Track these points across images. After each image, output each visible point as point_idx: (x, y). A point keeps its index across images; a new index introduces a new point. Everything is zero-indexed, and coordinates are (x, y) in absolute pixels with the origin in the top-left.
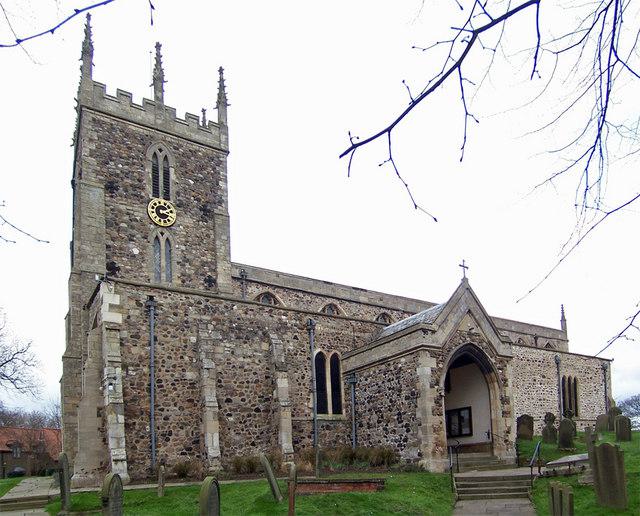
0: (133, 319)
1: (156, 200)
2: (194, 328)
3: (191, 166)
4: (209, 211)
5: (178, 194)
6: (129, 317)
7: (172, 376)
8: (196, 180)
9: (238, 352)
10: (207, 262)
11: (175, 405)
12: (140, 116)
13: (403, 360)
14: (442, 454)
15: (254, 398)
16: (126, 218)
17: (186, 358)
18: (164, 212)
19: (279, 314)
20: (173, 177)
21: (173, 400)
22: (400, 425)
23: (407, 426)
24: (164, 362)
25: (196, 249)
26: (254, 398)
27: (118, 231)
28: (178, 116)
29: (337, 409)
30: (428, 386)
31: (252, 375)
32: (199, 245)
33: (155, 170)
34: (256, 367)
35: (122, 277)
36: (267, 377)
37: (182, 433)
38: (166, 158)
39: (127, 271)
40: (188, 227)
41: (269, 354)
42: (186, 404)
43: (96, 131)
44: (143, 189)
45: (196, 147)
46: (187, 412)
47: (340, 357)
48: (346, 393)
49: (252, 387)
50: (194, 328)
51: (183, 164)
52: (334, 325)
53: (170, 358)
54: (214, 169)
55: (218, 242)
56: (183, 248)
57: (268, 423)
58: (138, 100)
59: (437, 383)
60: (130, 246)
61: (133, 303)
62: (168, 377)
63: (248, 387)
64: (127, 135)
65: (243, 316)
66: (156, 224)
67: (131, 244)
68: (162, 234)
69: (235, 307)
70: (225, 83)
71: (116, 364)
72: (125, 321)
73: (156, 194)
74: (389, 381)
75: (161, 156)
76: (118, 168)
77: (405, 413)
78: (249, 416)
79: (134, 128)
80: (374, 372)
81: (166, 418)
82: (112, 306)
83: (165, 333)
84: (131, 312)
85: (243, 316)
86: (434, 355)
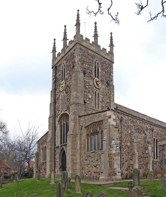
5: (101, 77)
6: (117, 123)
8: (105, 72)
20: (100, 70)
35: (87, 106)
36: (144, 146)
37: (126, 163)
39: (88, 104)
41: (145, 138)
45: (105, 60)
47: (158, 140)
50: (130, 128)
51: (102, 66)
54: (110, 68)
56: (102, 96)
60: (89, 95)
61: (118, 118)
66: (96, 87)
71: (118, 139)
72: (116, 125)
79: (90, 52)
81: (123, 159)
82: (114, 119)
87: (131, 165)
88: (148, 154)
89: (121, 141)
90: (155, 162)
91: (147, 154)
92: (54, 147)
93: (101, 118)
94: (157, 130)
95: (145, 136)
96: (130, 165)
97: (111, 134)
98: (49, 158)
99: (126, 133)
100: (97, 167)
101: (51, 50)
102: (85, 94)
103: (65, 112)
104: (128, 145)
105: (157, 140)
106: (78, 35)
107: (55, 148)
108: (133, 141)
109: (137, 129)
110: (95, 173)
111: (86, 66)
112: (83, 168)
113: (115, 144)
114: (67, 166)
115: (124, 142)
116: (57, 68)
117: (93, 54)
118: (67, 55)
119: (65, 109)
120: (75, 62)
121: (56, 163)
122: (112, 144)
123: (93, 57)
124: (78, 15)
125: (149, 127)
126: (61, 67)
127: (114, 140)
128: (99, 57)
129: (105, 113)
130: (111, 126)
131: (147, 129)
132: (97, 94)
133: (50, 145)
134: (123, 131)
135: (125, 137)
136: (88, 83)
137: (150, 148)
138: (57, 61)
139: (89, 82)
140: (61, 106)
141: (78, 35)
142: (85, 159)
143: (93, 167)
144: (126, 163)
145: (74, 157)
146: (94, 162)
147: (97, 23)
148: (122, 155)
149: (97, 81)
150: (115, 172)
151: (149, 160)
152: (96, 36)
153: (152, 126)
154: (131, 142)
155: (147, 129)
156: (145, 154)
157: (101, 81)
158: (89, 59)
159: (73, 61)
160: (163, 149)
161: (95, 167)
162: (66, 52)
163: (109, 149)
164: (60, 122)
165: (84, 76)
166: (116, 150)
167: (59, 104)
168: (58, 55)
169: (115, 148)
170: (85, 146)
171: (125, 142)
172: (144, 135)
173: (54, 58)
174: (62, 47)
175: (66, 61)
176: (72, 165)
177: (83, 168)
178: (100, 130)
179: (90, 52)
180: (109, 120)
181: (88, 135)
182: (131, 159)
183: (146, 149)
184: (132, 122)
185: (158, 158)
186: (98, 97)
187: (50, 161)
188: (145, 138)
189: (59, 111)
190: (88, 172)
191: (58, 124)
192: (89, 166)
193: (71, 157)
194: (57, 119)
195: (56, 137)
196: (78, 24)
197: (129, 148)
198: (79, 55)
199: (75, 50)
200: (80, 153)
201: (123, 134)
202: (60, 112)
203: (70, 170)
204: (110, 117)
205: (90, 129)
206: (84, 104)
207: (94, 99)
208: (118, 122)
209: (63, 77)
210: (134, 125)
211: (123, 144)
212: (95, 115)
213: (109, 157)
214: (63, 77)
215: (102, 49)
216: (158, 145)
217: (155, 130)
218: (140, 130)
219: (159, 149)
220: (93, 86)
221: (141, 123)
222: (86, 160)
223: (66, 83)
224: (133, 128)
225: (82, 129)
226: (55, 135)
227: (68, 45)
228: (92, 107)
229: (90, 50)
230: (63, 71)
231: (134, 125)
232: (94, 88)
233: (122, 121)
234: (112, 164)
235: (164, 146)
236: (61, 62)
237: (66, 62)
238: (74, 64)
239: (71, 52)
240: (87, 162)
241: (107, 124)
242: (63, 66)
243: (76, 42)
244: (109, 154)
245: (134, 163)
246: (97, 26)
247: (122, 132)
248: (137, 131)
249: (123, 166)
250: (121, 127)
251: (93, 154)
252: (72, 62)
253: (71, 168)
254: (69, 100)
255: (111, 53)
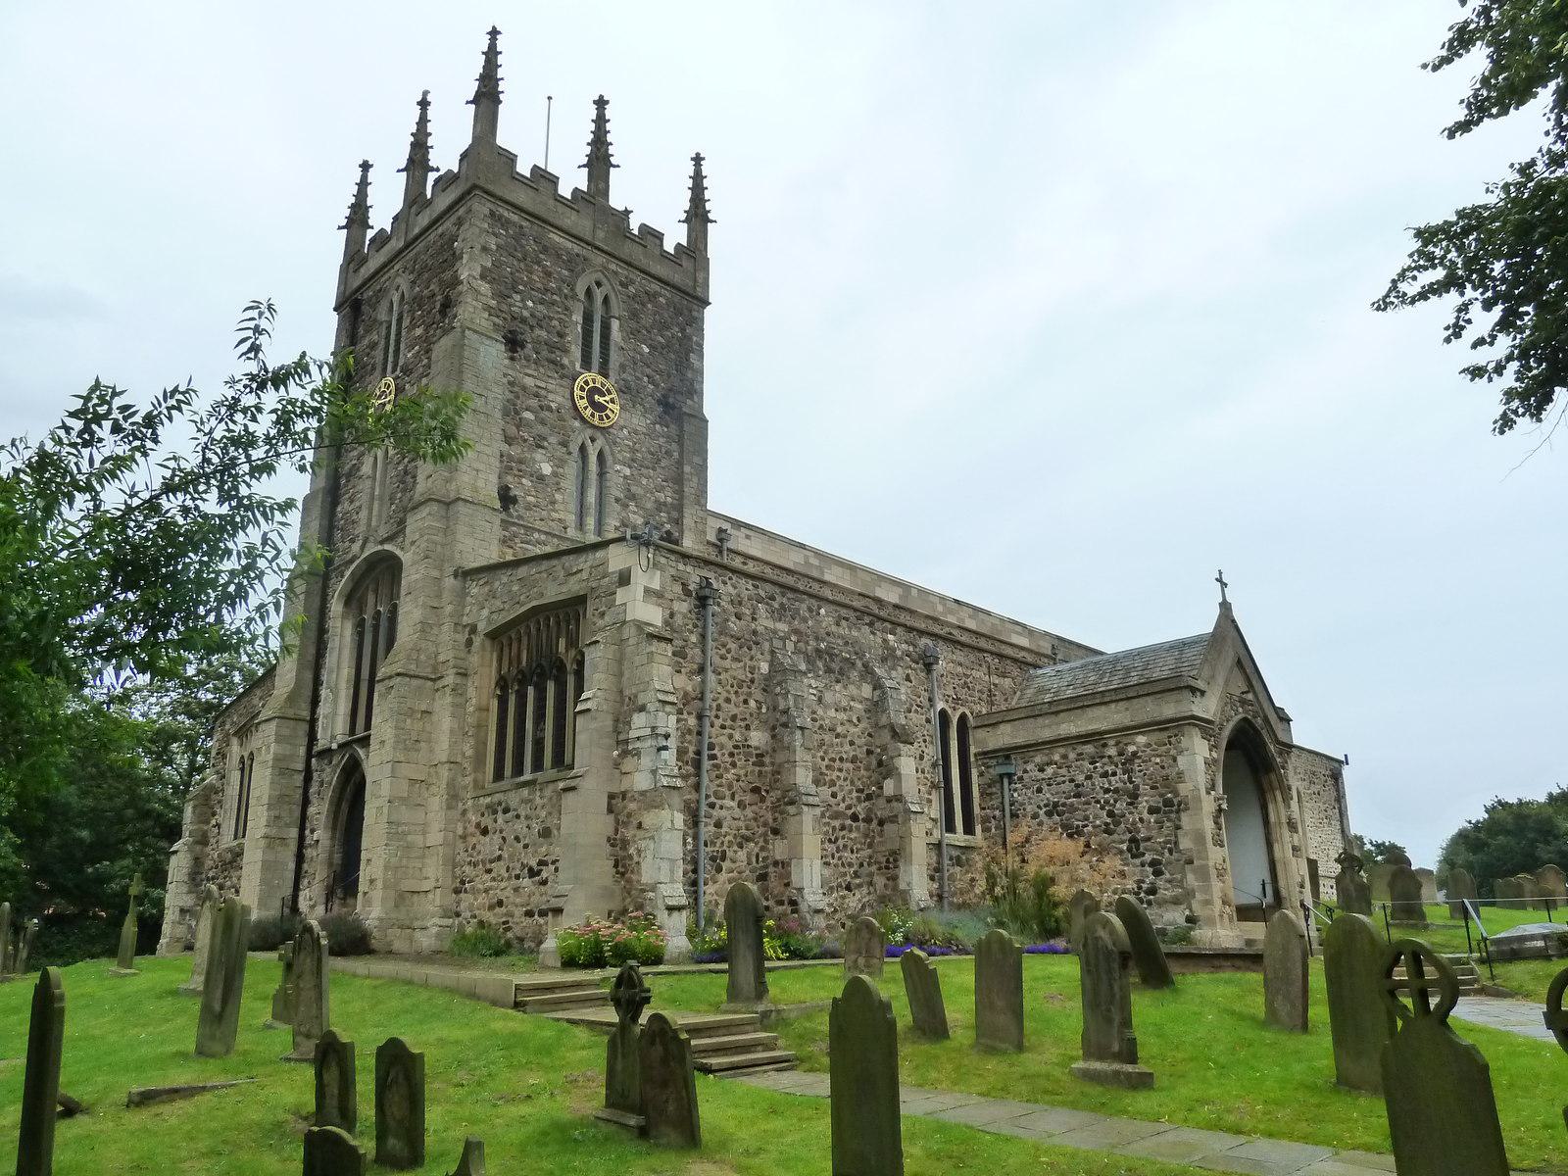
0: (679, 620)
1: (588, 376)
2: (766, 646)
3: (647, 320)
4: (673, 407)
5: (623, 367)
6: (672, 615)
7: (731, 737)
9: (828, 697)
10: (665, 504)
11: (733, 798)
12: (569, 220)
13: (1141, 739)
14: (1231, 920)
15: (850, 792)
16: (534, 402)
17: (752, 703)
18: (601, 400)
19: (883, 631)
21: (730, 787)
22: (1138, 861)
23: (1153, 863)
24: (719, 708)
25: (648, 477)
26: (850, 792)
27: (518, 427)
28: (665, 248)
29: (969, 829)
30: (1203, 791)
31: (847, 747)
32: (654, 469)
33: (588, 319)
34: (853, 730)
35: (520, 517)
36: (869, 752)
37: (742, 855)
38: (606, 300)
39: (529, 507)
40: (636, 432)
41: (876, 707)
42: (748, 798)
43: (494, 234)
44: (566, 351)
45: (655, 287)
46: (749, 812)
47: (971, 721)
48: (982, 794)
49: (848, 771)
50: (766, 646)
51: (634, 315)
52: (962, 660)
53: (728, 700)
54: (683, 330)
55: (687, 469)
56: (628, 472)
57: (870, 846)
58: (565, 190)
59: (1213, 787)
61: (678, 589)
62: (724, 739)
63: (840, 770)
64: (545, 250)
65: (834, 628)
66: (583, 420)
67: (539, 455)
68: (593, 440)
69: (822, 611)
70: (608, 126)
71: (668, 708)
72: (666, 623)
73: (587, 364)
74: (1105, 775)
75: (599, 295)
76: (526, 307)
77: (1148, 839)
78: (843, 828)
79: (557, 239)
80: (1065, 757)
81: (718, 825)
82: (647, 591)
83: (723, 651)
84: (677, 606)
85: (834, 628)
86: (1207, 735)
87: (776, 863)
88: (898, 798)
89: (700, 717)
90: (955, 853)
91: (889, 800)
92: (302, 751)
93: (573, 587)
94: (960, 664)
95: (877, 692)
96: (771, 869)
97: (627, 674)
98: (263, 821)
99: (738, 671)
100: (544, 875)
101: (342, 214)
102: (514, 451)
103: (387, 547)
104: (754, 742)
105: (963, 718)
106: (485, 150)
107: (309, 755)
108: (784, 719)
109: (818, 651)
110: (529, 914)
111: (525, 306)
112: (463, 882)
113: (648, 731)
114: (364, 873)
115: (723, 727)
116: (365, 308)
117: (577, 249)
118: (420, 246)
119: (383, 532)
120: (456, 282)
121: (309, 852)
122: (633, 734)
123: (575, 264)
124: (698, 179)
125: (904, 646)
126: (384, 306)
127: (642, 709)
128: (613, 267)
129: (600, 554)
130: (629, 632)
131: (889, 657)
132: (593, 459)
133: (279, 739)
134: (712, 653)
135: (733, 697)
136: (537, 395)
137: (907, 765)
138: (366, 271)
139: (543, 392)
140: (364, 514)
141: (485, 150)
142: (478, 825)
143: (517, 877)
144: (742, 855)
145: (405, 814)
146: (526, 846)
147: (607, 102)
148: (712, 806)
149: (595, 391)
150: (648, 909)
151: (904, 838)
152: (599, 160)
153: (925, 641)
154: (774, 728)
155: (889, 657)
156: (881, 802)
157: (620, 391)
158: (548, 274)
159: (447, 275)
160: (1001, 776)
161: (532, 873)
162: (417, 231)
163: (617, 765)
164: (354, 604)
165: (512, 359)
166: (654, 772)
167: (357, 504)
168: (372, 240)
169: (646, 761)
170: (485, 744)
171: (729, 723)
172: (866, 690)
173: (353, 258)
174: (396, 204)
175: (412, 277)
176: (386, 868)
177: (463, 882)
178: (572, 653)
179: (557, 239)
180: (621, 595)
181: (503, 683)
182: (776, 832)
183: (885, 769)
184: (780, 614)
185: (978, 828)
186: (602, 475)
187: (266, 837)
188: (876, 707)
189: (352, 541)
190: (491, 908)
191: (344, 617)
192: (499, 868)
193: (385, 810)
194: (340, 586)
195: (324, 692)
196: (487, 96)
197: (762, 764)
198: (485, 249)
199: (460, 223)
200: (451, 785)
201: (711, 677)
202: (356, 547)
203: (377, 894)
204: (624, 579)
205: (515, 646)
206: (498, 505)
207: (570, 484)
208: (683, 607)
209: (390, 359)
210: (796, 632)
211: (713, 733)
212: (545, 565)
213: (610, 810)
214: (390, 359)
215: (636, 232)
216: (973, 750)
217: (941, 666)
218: (834, 664)
219: (981, 774)
220: (567, 413)
221: (844, 623)
222: (485, 832)
223: (399, 390)
224: (790, 646)
225: (469, 643)
226: (317, 683)
227: (429, 196)
228: (556, 528)
229: (556, 228)
230: (394, 323)
231: (796, 632)
232: (577, 424)
233: (711, 601)
234: (631, 857)
235: (1008, 757)
236: (386, 277)
237: (413, 282)
238: (453, 295)
239: (440, 230)
240: (489, 846)
241: (606, 618)
242: (396, 299)
243: (469, 185)
244: (611, 797)
245: (796, 854)
246: (608, 114)
247: (709, 669)
248: (820, 664)
249: (719, 870)
250: (703, 636)
251: (525, 792)
252: (441, 281)
253: (379, 884)
254: (409, 479)
255: (695, 252)
